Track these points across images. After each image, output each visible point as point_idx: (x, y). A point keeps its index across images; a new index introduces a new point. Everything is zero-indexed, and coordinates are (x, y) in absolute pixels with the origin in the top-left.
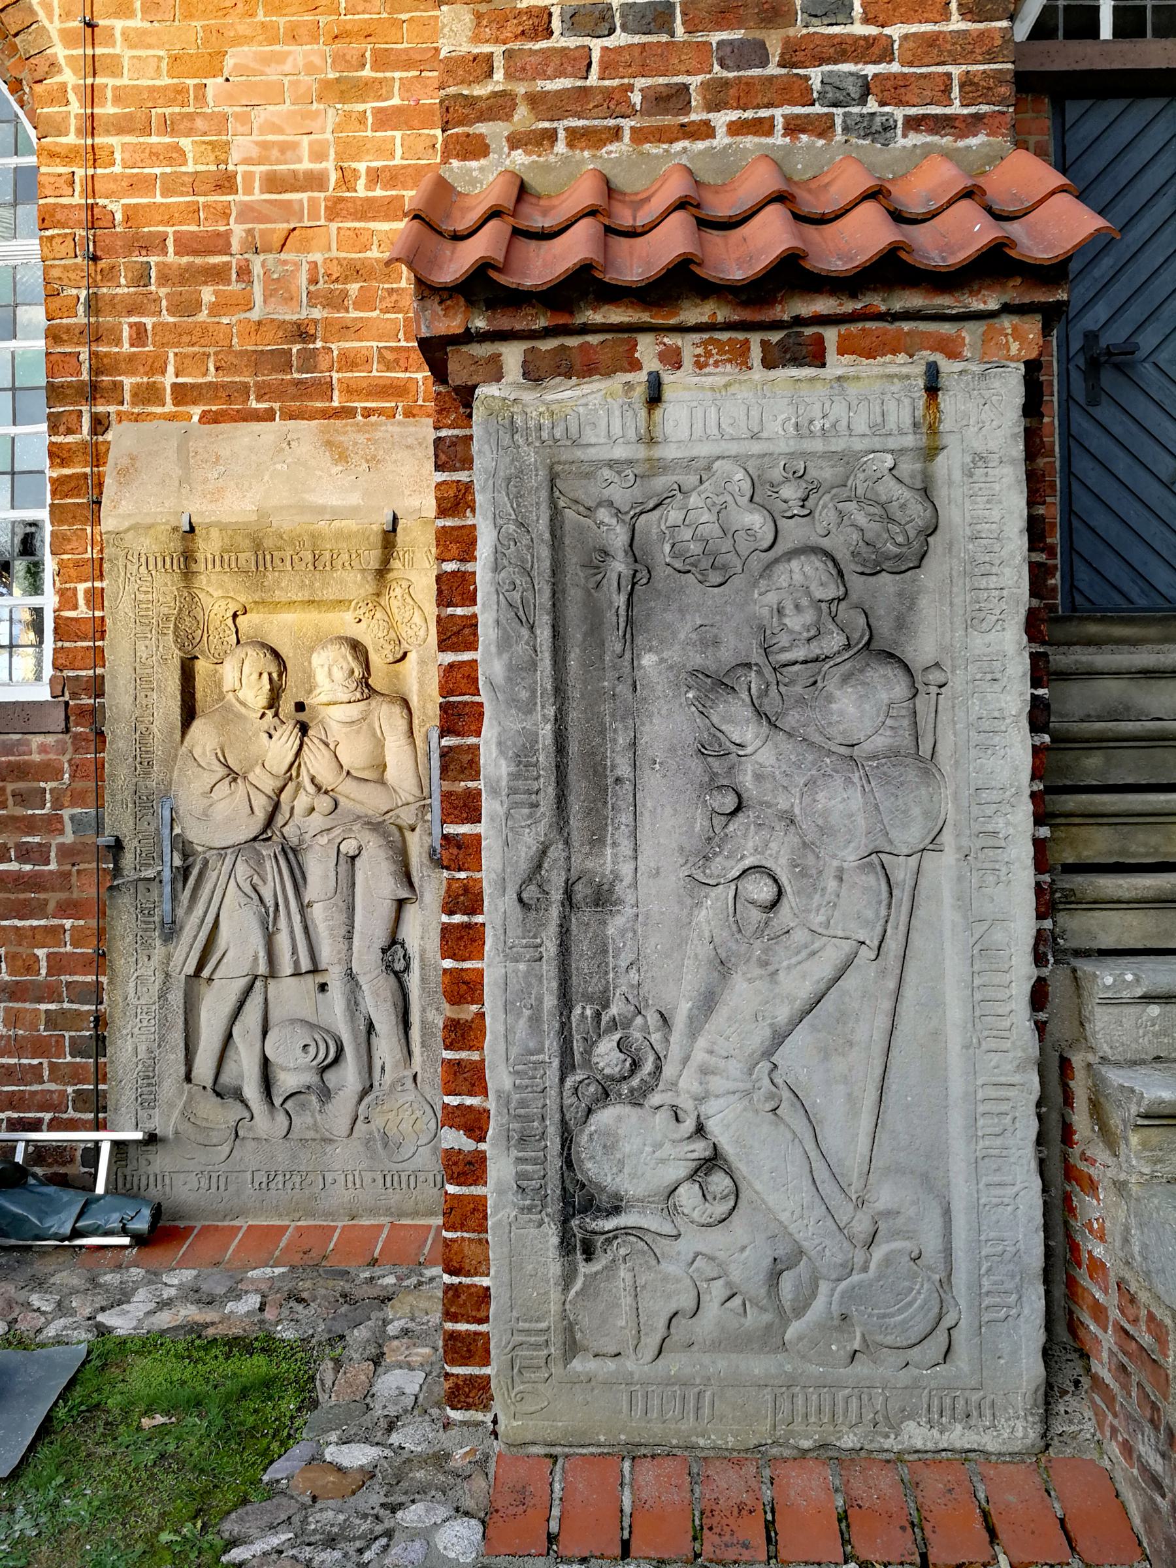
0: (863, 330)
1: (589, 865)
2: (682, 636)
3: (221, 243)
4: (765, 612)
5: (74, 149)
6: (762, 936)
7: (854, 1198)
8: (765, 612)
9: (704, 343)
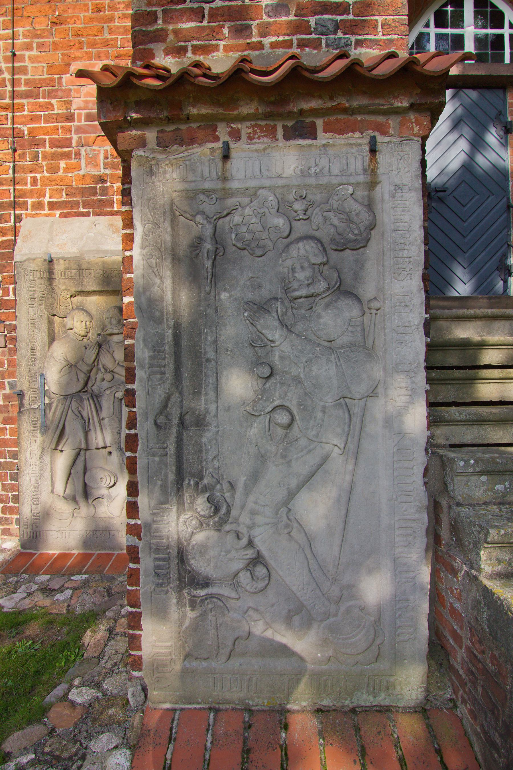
0: (337, 119)
1: (193, 405)
2: (242, 283)
3: (68, 143)
4: (286, 270)
5: (8, 105)
6: (283, 442)
7: (330, 578)
8: (286, 270)
9: (253, 127)
